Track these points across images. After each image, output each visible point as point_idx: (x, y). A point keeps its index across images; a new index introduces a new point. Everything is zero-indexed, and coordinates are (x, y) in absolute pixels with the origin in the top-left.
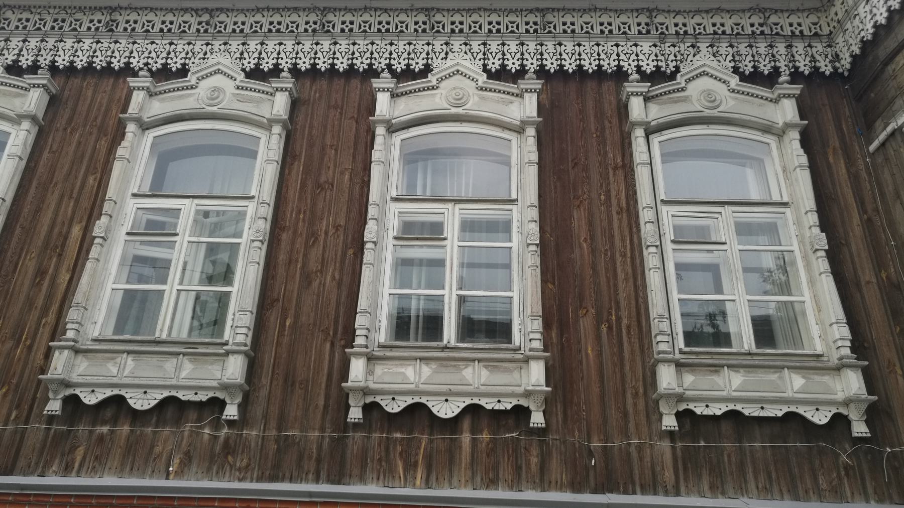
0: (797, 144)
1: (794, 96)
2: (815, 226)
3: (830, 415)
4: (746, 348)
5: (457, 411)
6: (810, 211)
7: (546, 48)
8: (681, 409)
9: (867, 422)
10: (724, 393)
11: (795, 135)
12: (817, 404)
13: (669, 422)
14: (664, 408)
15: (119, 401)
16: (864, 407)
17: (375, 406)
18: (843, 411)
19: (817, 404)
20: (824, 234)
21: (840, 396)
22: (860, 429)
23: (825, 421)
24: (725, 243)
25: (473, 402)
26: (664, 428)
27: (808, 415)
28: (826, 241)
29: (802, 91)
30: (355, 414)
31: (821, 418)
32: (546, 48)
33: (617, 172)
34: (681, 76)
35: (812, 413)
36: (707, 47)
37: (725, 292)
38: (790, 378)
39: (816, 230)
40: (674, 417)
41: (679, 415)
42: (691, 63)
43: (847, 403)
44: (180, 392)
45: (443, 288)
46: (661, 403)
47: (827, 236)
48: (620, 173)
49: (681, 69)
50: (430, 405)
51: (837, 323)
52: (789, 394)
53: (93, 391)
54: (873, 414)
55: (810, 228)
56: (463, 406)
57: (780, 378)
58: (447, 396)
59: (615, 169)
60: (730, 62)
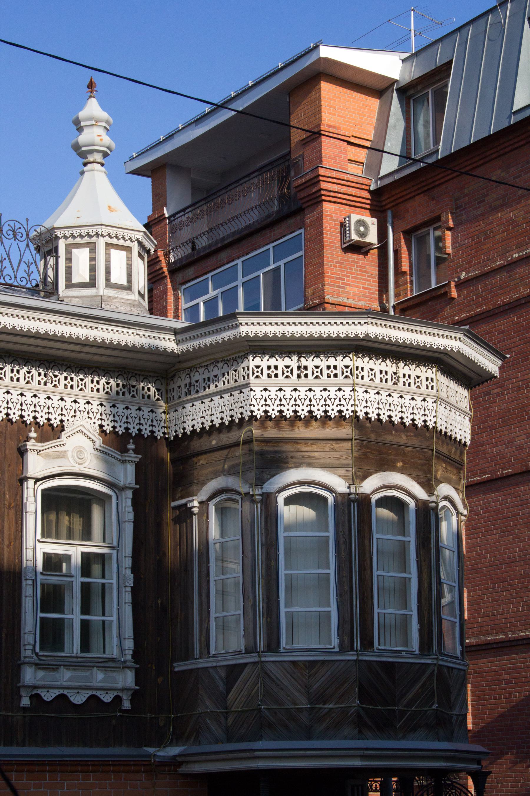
0: (129, 502)
1: (135, 462)
2: (129, 568)
3: (113, 696)
4: (75, 652)
5: (84, 699)
6: (128, 557)
7: (254, 393)
8: (33, 693)
9: (131, 701)
10: (59, 683)
11: (129, 494)
12: (107, 690)
13: (25, 701)
14: (23, 693)
15: (62, 697)
16: (131, 692)
17: (38, 696)
18: (120, 694)
19: (107, 690)
20: (133, 575)
21: (120, 685)
22: (127, 704)
23: (110, 700)
24: (72, 576)
25: (93, 693)
26: (22, 705)
27: (101, 697)
28: (133, 581)
29: (140, 459)
30: (25, 701)
31: (107, 698)
32: (254, 393)
33: (10, 511)
34: (64, 434)
35: (103, 695)
36: (149, 412)
37: (66, 612)
38: (97, 673)
39: (129, 572)
40: (28, 698)
41: (31, 697)
42: (73, 423)
43: (123, 690)
44: (98, 692)
45: (286, 612)
46: (21, 689)
47: (134, 578)
48: (12, 512)
49: (66, 429)
50: (69, 695)
51: (128, 638)
52: (94, 684)
53: (78, 692)
54: (135, 696)
55: (126, 568)
56: (87, 696)
57: (91, 674)
58: (79, 689)
59: (9, 508)
60: (149, 426)
